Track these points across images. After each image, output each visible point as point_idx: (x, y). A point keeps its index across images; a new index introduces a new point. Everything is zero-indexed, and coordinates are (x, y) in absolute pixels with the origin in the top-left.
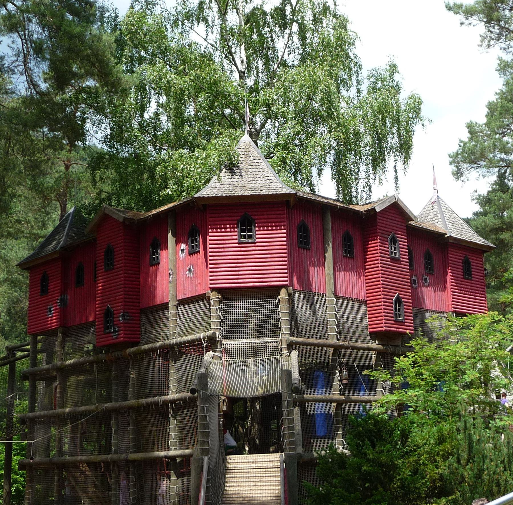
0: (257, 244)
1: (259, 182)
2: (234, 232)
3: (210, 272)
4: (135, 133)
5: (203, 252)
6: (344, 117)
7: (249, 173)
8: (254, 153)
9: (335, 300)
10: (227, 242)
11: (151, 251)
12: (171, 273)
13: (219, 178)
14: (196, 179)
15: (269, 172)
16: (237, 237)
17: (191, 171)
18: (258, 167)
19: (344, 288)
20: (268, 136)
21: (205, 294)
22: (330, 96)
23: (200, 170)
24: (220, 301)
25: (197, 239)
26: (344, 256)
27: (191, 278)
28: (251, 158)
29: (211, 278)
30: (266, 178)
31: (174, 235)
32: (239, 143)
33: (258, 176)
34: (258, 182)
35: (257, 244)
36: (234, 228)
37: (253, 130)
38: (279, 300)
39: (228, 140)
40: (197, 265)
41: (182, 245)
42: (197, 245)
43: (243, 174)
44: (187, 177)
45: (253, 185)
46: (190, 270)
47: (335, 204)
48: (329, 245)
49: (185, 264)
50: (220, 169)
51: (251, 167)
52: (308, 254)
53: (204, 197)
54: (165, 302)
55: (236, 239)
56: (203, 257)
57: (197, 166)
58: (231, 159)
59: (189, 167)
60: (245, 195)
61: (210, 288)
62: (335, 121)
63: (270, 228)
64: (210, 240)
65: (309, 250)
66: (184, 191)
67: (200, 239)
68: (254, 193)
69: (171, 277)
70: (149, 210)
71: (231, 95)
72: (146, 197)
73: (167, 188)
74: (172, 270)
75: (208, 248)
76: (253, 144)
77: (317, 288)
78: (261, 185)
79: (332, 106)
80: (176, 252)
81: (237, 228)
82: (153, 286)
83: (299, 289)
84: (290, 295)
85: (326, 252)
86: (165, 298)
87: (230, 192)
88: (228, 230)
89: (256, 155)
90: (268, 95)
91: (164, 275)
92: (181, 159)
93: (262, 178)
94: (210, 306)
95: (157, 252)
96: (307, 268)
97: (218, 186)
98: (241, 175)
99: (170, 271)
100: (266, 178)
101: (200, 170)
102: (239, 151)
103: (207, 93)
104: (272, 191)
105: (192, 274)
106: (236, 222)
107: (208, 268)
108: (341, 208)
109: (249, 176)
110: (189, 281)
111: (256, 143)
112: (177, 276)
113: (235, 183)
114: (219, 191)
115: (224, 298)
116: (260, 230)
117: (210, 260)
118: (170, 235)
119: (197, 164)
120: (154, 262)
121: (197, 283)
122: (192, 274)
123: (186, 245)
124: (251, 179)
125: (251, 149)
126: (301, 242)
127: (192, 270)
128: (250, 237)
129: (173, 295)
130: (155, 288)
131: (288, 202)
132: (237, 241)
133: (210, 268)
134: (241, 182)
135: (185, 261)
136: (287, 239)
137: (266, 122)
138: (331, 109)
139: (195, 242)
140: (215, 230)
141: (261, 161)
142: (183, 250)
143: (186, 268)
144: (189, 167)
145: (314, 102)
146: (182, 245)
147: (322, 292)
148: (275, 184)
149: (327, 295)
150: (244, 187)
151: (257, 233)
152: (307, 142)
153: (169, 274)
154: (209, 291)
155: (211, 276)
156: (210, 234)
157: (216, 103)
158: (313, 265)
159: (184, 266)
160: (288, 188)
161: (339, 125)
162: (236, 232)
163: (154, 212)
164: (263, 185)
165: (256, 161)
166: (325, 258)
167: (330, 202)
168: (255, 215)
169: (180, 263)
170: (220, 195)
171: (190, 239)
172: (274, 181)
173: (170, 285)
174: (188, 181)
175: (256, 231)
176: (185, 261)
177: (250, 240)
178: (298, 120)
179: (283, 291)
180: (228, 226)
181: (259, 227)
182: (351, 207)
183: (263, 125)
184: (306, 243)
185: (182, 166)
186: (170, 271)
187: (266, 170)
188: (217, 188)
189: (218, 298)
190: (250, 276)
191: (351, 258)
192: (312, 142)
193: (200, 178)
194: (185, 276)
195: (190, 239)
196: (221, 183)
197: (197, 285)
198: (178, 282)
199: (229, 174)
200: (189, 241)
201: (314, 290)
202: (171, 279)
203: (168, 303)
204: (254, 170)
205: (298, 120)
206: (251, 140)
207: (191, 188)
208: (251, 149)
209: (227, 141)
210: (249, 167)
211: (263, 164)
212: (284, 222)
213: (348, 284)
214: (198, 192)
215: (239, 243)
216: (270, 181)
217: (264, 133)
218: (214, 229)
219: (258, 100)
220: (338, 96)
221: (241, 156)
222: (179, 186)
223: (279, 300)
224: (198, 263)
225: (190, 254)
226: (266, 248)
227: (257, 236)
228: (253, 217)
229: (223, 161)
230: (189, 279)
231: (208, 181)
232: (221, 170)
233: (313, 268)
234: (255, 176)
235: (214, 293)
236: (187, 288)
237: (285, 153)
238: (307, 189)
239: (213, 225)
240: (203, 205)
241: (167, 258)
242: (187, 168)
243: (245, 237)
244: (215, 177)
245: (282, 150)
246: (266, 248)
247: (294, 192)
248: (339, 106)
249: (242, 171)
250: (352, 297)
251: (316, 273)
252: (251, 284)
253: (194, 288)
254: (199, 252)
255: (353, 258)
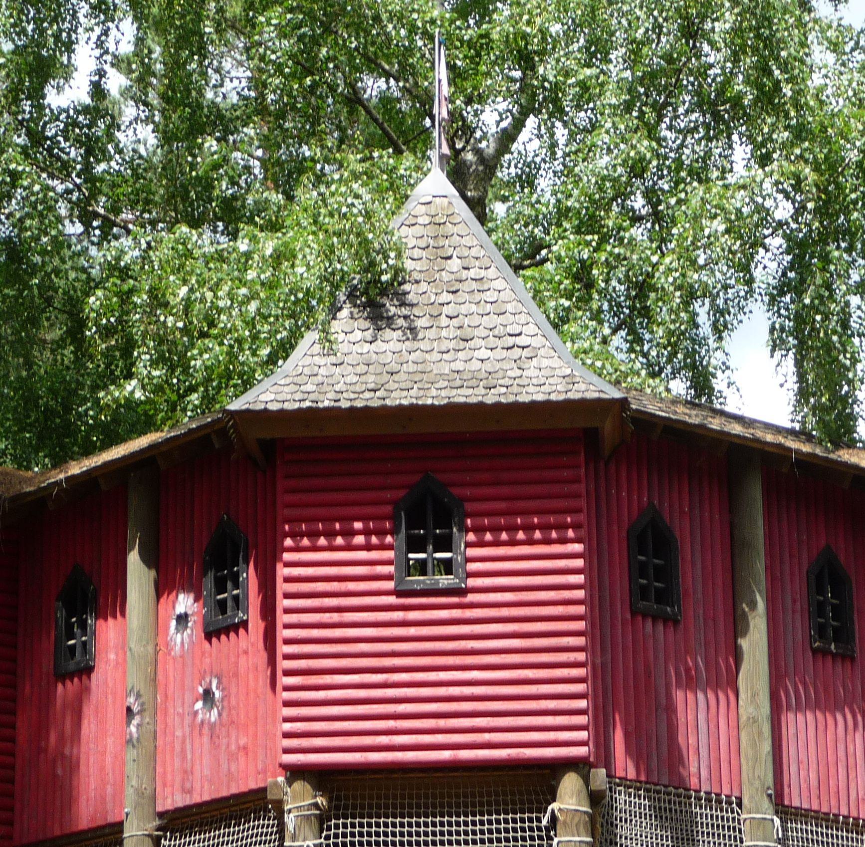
0: (471, 598)
1: (484, 353)
2: (383, 547)
3: (287, 704)
4: (9, 161)
5: (262, 625)
6: (822, 103)
7: (444, 321)
8: (467, 241)
9: (777, 821)
10: (352, 586)
11: (62, 624)
12: (135, 709)
13: (327, 340)
14: (240, 341)
15: (523, 318)
16: (390, 569)
17: (220, 311)
18: (477, 297)
19: (813, 775)
20: (527, 180)
21: (264, 790)
22: (769, 20)
23: (253, 307)
24: (322, 820)
25: (236, 575)
26: (815, 651)
27: (212, 726)
28: (455, 264)
29: (287, 727)
30: (510, 341)
31: (149, 559)
32: (410, 205)
33: (476, 332)
34: (477, 354)
35: (471, 598)
36: (381, 533)
37: (469, 157)
38: (554, 819)
39: (362, 191)
40: (236, 675)
41: (181, 597)
42: (236, 598)
43: (420, 323)
44: (203, 335)
45: (459, 366)
46: (208, 695)
47: (780, 446)
48: (753, 605)
49: (188, 671)
50: (333, 305)
51: (450, 297)
52: (671, 638)
53: (266, 410)
54: (111, 819)
55: (389, 577)
56: (261, 644)
57: (244, 291)
58: (372, 264)
59: (209, 295)
60: (425, 407)
61: (285, 767)
62: (787, 116)
63: (521, 535)
64: (288, 580)
65: (676, 622)
66: (192, 389)
67: (250, 576)
68: (461, 396)
69: (135, 721)
70: (59, 461)
71: (384, 17)
72: (49, 413)
73: (129, 376)
74: (138, 696)
75: (279, 611)
76: (462, 209)
77: (704, 773)
78: (488, 366)
79: (777, 59)
80: (157, 627)
81: (394, 532)
82: (63, 757)
83: (631, 774)
84: (595, 798)
85: (744, 633)
86: (109, 806)
87: (368, 395)
88: (360, 539)
89: (474, 252)
90: (526, 17)
91: (110, 715)
92: (182, 266)
93: (492, 342)
94: (282, 839)
95: (83, 625)
96: (669, 696)
97: (322, 371)
98: (413, 330)
99: (131, 700)
100: (510, 341)
101: (253, 307)
102: (408, 236)
103: (291, 10)
104: (531, 389)
105: (215, 712)
106: (388, 509)
107: (279, 688)
108: (806, 463)
109: (444, 333)
110: (206, 739)
111: (478, 208)
112: (159, 718)
113: (389, 357)
114: (325, 388)
115: (337, 808)
116: (481, 544)
117: (287, 657)
118: (134, 558)
119: (242, 282)
120: (72, 666)
121: (233, 747)
122: (215, 712)
123: (196, 600)
124: (452, 345)
125: (455, 229)
126: (644, 592)
127: (218, 694)
128: (447, 567)
129: (139, 793)
130: (73, 767)
131: (591, 436)
132: (390, 585)
133: (287, 689)
134: (413, 357)
135: (189, 662)
136: (589, 578)
137: (519, 124)
138: (770, 73)
139: (229, 585)
140: (306, 542)
141: (492, 273)
142: (182, 619)
143: (194, 689)
144: (209, 295)
145: (706, 48)
146: (181, 597)
147: (726, 791)
148: (545, 363)
149: (745, 801)
150: (421, 375)
151: (472, 552)
152: (673, 201)
153: (129, 710)
154: (281, 779)
155: (286, 720)
156: (287, 556)
157: (324, 51)
158: (691, 683)
159: (188, 682)
160: (595, 379)
161: (800, 133)
162: (390, 547)
163: (76, 469)
164: (498, 366)
165: (472, 273)
166: (737, 655)
167: (759, 434)
168: (463, 485)
169: (170, 667)
170: (327, 403)
171: (211, 575)
172: (542, 352)
173: (131, 754)
174: (207, 350)
175: (468, 545)
176: (189, 662)
177: (445, 581)
178: (642, 113)
179: (570, 784)
180: (358, 525)
181: (479, 530)
182: (845, 456)
183: (507, 138)
184: (663, 597)
185: (184, 290)
186: (131, 700)
187: (510, 308)
188: (319, 379)
189: (316, 806)
190: (442, 723)
191: (844, 657)
192: (695, 202)
193: (255, 337)
194: (188, 720)
195: (211, 575)
196: (333, 359)
197: (232, 757)
198: (160, 742)
199: (367, 324)
200: (209, 582)
201: (694, 782)
202: (133, 729)
203: (121, 824)
204: (463, 309)
205: (642, 113)
206: (452, 191)
207: (220, 377)
208: (455, 229)
209: (357, 196)
210: (445, 297)
211: (499, 284)
212: (578, 511)
213: (832, 758)
214: (246, 390)
215: (398, 593)
216: (526, 353)
217: (513, 170)
218: (302, 535)
219: (486, 35)
220: (799, 19)
221: (416, 253)
222: (172, 369)
223: (554, 819)
224: (242, 670)
225: (211, 634)
226: (505, 612)
227: (472, 567)
228: (456, 491)
229: (344, 274)
230: (206, 730)
231: (284, 349)
232: (334, 310)
233: (690, 696)
234: (468, 333)
235: (298, 785)
236: (197, 768)
237: (588, 244)
238: (679, 387)
239: (300, 520)
240: (261, 442)
241: (123, 646)
242: (203, 300)
243: (422, 568)
244: (311, 337)
245: (578, 231)
246: (505, 612)
247: (617, 394)
248: (802, 62)
249: (416, 311)
250: (844, 811)
251: (702, 716)
252: (446, 755)
253: (225, 766)
254: (244, 624)
255: (852, 659)
